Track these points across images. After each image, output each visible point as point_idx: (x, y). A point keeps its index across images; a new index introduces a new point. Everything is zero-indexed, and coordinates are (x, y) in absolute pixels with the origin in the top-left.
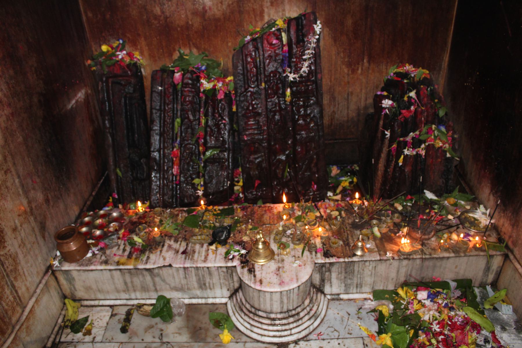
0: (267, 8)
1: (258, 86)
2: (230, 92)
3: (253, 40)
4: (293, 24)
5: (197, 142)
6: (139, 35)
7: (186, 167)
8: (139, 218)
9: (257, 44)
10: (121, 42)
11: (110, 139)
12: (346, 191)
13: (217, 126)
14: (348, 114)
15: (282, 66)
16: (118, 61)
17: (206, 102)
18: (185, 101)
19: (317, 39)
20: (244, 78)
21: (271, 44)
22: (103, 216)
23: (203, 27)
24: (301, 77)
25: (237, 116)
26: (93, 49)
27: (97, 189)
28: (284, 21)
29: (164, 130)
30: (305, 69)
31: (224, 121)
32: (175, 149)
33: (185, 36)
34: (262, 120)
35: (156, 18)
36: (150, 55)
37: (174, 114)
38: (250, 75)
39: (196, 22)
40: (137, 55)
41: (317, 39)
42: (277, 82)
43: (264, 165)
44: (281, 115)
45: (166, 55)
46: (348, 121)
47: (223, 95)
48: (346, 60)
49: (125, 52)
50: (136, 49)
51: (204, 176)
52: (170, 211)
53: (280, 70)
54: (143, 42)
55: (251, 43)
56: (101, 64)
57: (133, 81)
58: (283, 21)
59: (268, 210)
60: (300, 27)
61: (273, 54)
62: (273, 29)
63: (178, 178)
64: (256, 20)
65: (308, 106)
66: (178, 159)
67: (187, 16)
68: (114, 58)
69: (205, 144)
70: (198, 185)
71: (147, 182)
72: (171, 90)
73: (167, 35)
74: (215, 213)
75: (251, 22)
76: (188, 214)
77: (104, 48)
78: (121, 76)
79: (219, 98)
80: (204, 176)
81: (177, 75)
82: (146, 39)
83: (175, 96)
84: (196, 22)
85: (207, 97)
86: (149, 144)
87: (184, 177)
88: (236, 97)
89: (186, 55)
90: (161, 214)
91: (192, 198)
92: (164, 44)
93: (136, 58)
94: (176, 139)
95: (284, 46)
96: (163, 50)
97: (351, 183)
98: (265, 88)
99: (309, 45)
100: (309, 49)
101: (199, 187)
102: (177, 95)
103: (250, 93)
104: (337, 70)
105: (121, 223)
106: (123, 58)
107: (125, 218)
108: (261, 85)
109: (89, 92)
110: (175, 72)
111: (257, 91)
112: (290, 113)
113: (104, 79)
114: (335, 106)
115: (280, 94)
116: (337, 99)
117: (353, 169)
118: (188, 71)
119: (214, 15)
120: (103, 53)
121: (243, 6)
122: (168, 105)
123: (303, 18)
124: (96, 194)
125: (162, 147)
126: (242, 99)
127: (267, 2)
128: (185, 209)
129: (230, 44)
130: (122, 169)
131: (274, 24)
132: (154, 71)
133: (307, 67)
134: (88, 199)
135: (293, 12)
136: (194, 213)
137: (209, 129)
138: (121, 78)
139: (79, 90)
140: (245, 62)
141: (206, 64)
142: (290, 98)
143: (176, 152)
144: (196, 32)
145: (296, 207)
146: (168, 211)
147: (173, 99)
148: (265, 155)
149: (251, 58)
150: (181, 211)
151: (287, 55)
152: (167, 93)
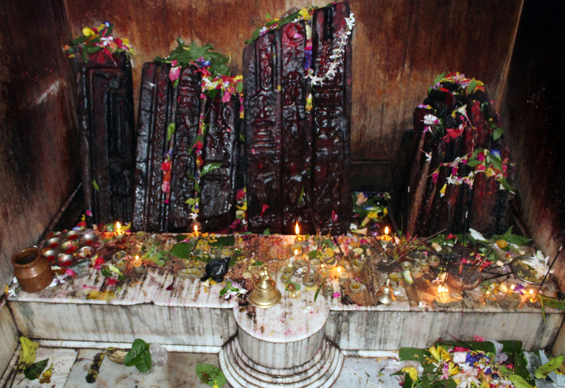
4: (321, 15)
5: (194, 153)
6: (130, 18)
7: (178, 183)
8: (116, 243)
9: (275, 38)
10: (107, 25)
13: (220, 135)
16: (102, 49)
17: (208, 106)
18: (182, 103)
19: (348, 36)
20: (256, 78)
21: (291, 39)
22: (73, 238)
24: (326, 80)
25: (245, 124)
26: (73, 32)
27: (67, 204)
29: (154, 136)
30: (331, 71)
31: (228, 130)
32: (166, 161)
33: (186, 22)
34: (275, 130)
36: (142, 43)
37: (167, 117)
40: (126, 42)
41: (348, 36)
42: (296, 86)
44: (299, 126)
45: (162, 44)
46: (380, 139)
47: (230, 97)
48: (383, 63)
49: (111, 38)
50: (126, 35)
51: (199, 195)
52: (156, 236)
53: (301, 71)
54: (134, 27)
55: (267, 36)
56: (81, 51)
57: (119, 74)
58: (309, 11)
59: (277, 242)
61: (293, 51)
62: (296, 20)
63: (168, 196)
64: (275, 8)
65: (332, 118)
66: (169, 172)
68: (98, 45)
70: (192, 206)
71: (129, 199)
74: (211, 241)
76: (178, 241)
77: (87, 32)
78: (105, 67)
79: (224, 101)
81: (174, 70)
83: (170, 96)
86: (134, 153)
87: (175, 195)
88: (245, 101)
89: (187, 46)
91: (184, 222)
92: (160, 31)
93: (125, 46)
96: (158, 38)
97: (380, 214)
98: (281, 92)
99: (338, 42)
102: (173, 95)
104: (371, 75)
105: (94, 247)
106: (108, 45)
108: (277, 89)
109: (65, 84)
111: (271, 95)
112: (310, 125)
113: (84, 70)
114: (366, 119)
116: (368, 111)
117: (383, 198)
118: (188, 65)
122: (161, 105)
123: (333, 9)
124: (66, 210)
125: (150, 157)
128: (175, 235)
129: (241, 36)
130: (100, 182)
132: (145, 64)
133: (334, 69)
134: (56, 216)
136: (185, 241)
137: (209, 139)
138: (104, 70)
139: (53, 81)
140: (258, 59)
141: (210, 58)
142: (311, 106)
143: (167, 165)
144: (200, 19)
145: (310, 241)
146: (154, 236)
147: (168, 99)
148: (276, 174)
149: (267, 55)
150: (169, 236)
151: (311, 53)
152: (161, 91)
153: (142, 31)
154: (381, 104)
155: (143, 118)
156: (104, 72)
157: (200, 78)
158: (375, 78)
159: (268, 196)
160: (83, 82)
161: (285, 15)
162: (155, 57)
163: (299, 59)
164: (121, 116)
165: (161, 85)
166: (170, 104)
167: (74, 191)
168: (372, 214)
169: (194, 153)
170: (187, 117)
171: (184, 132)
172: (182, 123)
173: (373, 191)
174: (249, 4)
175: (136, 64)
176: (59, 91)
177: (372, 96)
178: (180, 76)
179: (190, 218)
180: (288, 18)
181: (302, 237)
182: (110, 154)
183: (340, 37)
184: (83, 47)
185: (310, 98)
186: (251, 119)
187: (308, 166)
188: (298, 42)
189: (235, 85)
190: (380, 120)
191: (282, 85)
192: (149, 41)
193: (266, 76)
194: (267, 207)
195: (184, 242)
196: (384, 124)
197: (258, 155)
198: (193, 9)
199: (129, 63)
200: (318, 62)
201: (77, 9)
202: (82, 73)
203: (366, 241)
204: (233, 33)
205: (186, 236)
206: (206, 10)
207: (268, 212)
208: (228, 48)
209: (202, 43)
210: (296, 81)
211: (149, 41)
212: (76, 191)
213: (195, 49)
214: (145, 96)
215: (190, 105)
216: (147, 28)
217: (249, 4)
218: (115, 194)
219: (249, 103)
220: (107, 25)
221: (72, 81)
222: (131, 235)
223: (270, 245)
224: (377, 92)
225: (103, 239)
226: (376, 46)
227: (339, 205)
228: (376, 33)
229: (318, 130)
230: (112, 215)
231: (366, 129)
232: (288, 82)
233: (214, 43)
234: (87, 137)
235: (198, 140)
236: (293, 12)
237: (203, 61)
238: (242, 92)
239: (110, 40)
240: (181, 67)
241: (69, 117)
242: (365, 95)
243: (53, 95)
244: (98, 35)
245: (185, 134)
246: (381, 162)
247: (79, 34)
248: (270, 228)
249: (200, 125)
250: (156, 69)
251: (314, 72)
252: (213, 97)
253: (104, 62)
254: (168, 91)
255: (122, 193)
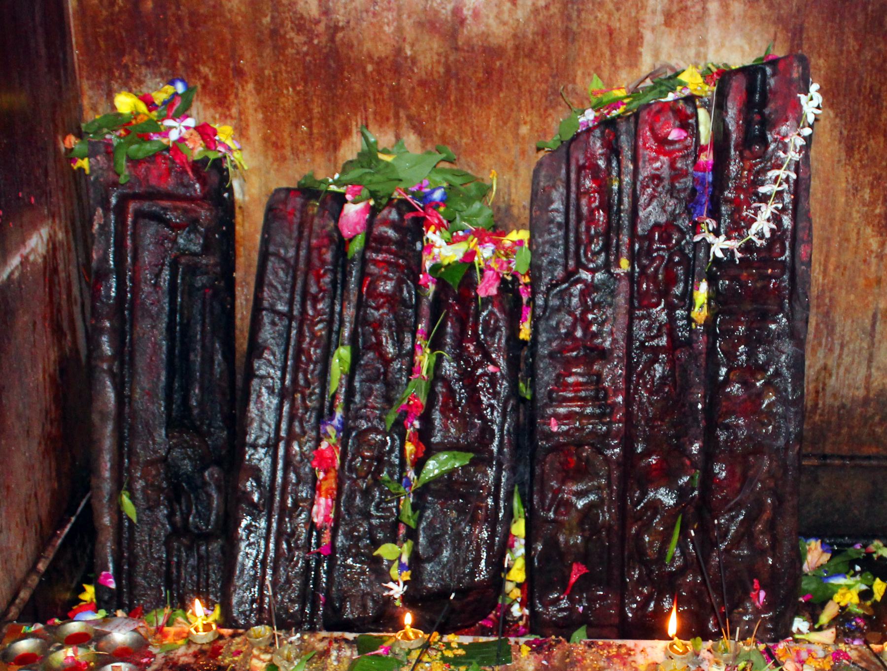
0: (653, 29)
1: (606, 267)
2: (515, 276)
3: (607, 125)
4: (738, 85)
5: (399, 427)
6: (239, 73)
7: (358, 501)
8: (195, 655)
9: (617, 138)
10: (180, 88)
11: (111, 395)
12: (850, 621)
13: (469, 379)
14: (868, 377)
15: (689, 211)
16: (168, 149)
17: (438, 304)
18: (373, 293)
19: (805, 138)
20: (566, 237)
21: (662, 141)
22: (78, 640)
23: (448, 70)
24: (749, 247)
25: (533, 354)
26: (86, 102)
27: (51, 553)
28: (707, 76)
29: (295, 380)
30: (762, 225)
31: (491, 368)
32: (324, 445)
33: (386, 90)
34: (612, 372)
35: (302, 25)
36: (266, 139)
37: (330, 332)
38: (588, 230)
39: (428, 53)
40: (225, 133)
41: (805, 138)
42: (671, 259)
43: (605, 516)
44: (672, 362)
45: (318, 144)
46: (866, 401)
47: (496, 284)
48: (878, 211)
49: (191, 122)
50: (225, 118)
51: (412, 534)
53: (684, 223)
54: (248, 95)
55: (597, 133)
56: (110, 152)
57: (204, 214)
58: (703, 75)
59: (618, 655)
60: (756, 96)
61: (666, 173)
62: (671, 97)
63: (326, 539)
64: (614, 64)
65: (760, 341)
66: (332, 474)
67: (400, 29)
69: (424, 435)
70: (391, 562)
71: (215, 546)
72: (329, 256)
73: (331, 80)
74: (449, 654)
75: (598, 70)
76: (361, 652)
77: (126, 103)
78: (169, 196)
79: (482, 294)
80: (412, 534)
81: (352, 210)
82: (260, 87)
83: (339, 276)
84: (428, 53)
85: (442, 285)
86: (236, 423)
87: (348, 535)
88: (534, 294)
89: (386, 152)
90: (272, 644)
91: (370, 604)
92: (316, 110)
93: (223, 144)
94: (332, 414)
95: (703, 149)
96: (310, 127)
97: (865, 595)
98: (630, 275)
99: (781, 154)
100: (779, 167)
101: (394, 572)
102: (346, 274)
103: (579, 286)
104: (847, 240)
105: (138, 664)
106: (182, 140)
107: (154, 650)
108: (619, 266)
109: (61, 236)
110: (346, 201)
111: (603, 283)
112: (702, 361)
113: (114, 201)
114: (831, 350)
115: (676, 296)
116: (838, 329)
117: (869, 555)
118: (391, 200)
119: (485, 36)
120: (117, 121)
121: (578, 16)
122: (315, 300)
123: (769, 70)
124: (48, 571)
125: (283, 434)
126: (554, 302)
127: (654, 12)
128: (350, 636)
129: (524, 130)
130: (139, 495)
131: (672, 80)
132: (278, 191)
133: (768, 220)
134: (23, 583)
135: (737, 48)
136: (381, 651)
137: (440, 388)
138: (167, 204)
139: (35, 226)
140: (573, 188)
141: (445, 185)
142: (705, 312)
143: (328, 454)
144: (422, 83)
145: (704, 654)
146: (295, 637)
147: (334, 282)
148: (609, 485)
149: (595, 179)
150: (336, 640)
151: (710, 178)
152: (317, 263)
153: (268, 108)
154: (870, 313)
155: (267, 334)
156: (165, 209)
157: (420, 235)
158: (857, 247)
159: (586, 540)
160: (109, 232)
161: (643, 81)
162: (298, 177)
163: (679, 191)
164: (203, 326)
165: (319, 248)
166: (338, 297)
167: (69, 521)
168: (844, 595)
169: (399, 427)
170: (385, 331)
171: (377, 374)
172: (368, 348)
173: (843, 536)
174: (548, 53)
175: (249, 191)
176: (48, 252)
177: (847, 292)
178: (370, 225)
179: (386, 594)
180: (652, 88)
181: (685, 645)
182: (170, 425)
183: (787, 140)
184: (115, 141)
185: (702, 293)
186: (550, 341)
187: (694, 466)
188: (679, 151)
189: (509, 252)
190: (865, 353)
191: (633, 258)
192: (286, 135)
193: (593, 232)
194: (584, 570)
195: (378, 655)
196: (874, 364)
197: (566, 433)
198: (406, 58)
199: (231, 190)
200: (728, 201)
201: (102, 44)
202: (106, 209)
203: (846, 656)
204: (505, 123)
205: (381, 640)
206: (439, 62)
207: (586, 584)
208: (488, 161)
209: (423, 147)
210: (668, 249)
211: (286, 135)
212: (73, 519)
213: (408, 160)
214: (276, 274)
215: (393, 300)
216: (283, 99)
217: (548, 53)
218: (180, 531)
219: (546, 301)
220: (180, 88)
221: (80, 231)
222: (233, 636)
223: (602, 664)
224: (861, 282)
225: (162, 646)
226: (863, 167)
227: (772, 566)
228: (864, 134)
229: (723, 371)
230: (168, 586)
231: (830, 375)
232: (650, 251)
233: (455, 145)
234: (113, 376)
235: (414, 391)
236: (663, 77)
237: (427, 190)
238: (527, 274)
239: (187, 128)
240: (372, 203)
241: (65, 325)
242: (831, 290)
243: (34, 264)
244: (155, 113)
245: (379, 374)
246: (865, 463)
247: (103, 108)
248: (590, 625)
249: (419, 352)
250: (304, 205)
251: (719, 224)
252: (455, 281)
253: (170, 184)
254: (335, 263)
255: (197, 527)
